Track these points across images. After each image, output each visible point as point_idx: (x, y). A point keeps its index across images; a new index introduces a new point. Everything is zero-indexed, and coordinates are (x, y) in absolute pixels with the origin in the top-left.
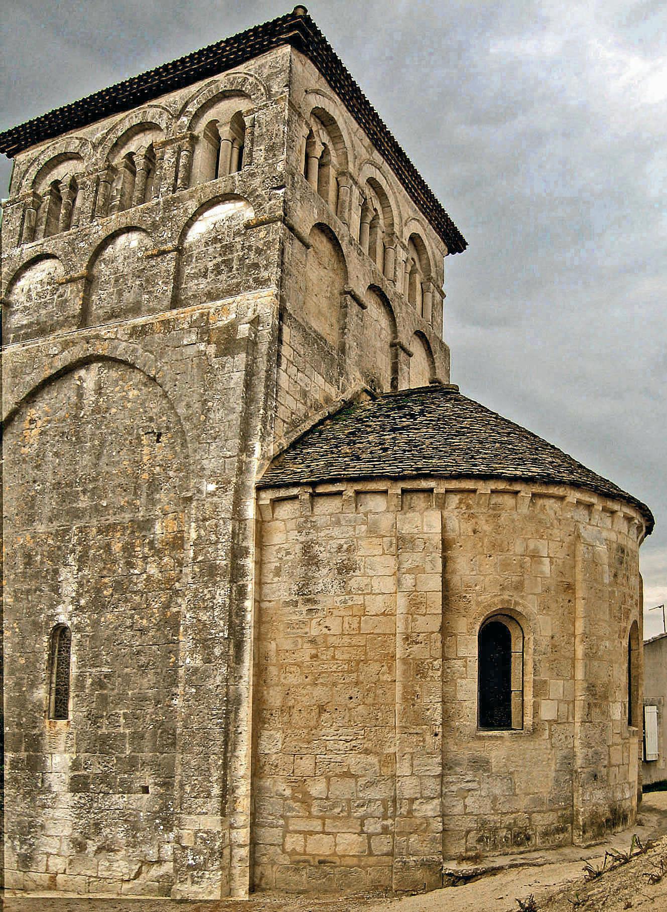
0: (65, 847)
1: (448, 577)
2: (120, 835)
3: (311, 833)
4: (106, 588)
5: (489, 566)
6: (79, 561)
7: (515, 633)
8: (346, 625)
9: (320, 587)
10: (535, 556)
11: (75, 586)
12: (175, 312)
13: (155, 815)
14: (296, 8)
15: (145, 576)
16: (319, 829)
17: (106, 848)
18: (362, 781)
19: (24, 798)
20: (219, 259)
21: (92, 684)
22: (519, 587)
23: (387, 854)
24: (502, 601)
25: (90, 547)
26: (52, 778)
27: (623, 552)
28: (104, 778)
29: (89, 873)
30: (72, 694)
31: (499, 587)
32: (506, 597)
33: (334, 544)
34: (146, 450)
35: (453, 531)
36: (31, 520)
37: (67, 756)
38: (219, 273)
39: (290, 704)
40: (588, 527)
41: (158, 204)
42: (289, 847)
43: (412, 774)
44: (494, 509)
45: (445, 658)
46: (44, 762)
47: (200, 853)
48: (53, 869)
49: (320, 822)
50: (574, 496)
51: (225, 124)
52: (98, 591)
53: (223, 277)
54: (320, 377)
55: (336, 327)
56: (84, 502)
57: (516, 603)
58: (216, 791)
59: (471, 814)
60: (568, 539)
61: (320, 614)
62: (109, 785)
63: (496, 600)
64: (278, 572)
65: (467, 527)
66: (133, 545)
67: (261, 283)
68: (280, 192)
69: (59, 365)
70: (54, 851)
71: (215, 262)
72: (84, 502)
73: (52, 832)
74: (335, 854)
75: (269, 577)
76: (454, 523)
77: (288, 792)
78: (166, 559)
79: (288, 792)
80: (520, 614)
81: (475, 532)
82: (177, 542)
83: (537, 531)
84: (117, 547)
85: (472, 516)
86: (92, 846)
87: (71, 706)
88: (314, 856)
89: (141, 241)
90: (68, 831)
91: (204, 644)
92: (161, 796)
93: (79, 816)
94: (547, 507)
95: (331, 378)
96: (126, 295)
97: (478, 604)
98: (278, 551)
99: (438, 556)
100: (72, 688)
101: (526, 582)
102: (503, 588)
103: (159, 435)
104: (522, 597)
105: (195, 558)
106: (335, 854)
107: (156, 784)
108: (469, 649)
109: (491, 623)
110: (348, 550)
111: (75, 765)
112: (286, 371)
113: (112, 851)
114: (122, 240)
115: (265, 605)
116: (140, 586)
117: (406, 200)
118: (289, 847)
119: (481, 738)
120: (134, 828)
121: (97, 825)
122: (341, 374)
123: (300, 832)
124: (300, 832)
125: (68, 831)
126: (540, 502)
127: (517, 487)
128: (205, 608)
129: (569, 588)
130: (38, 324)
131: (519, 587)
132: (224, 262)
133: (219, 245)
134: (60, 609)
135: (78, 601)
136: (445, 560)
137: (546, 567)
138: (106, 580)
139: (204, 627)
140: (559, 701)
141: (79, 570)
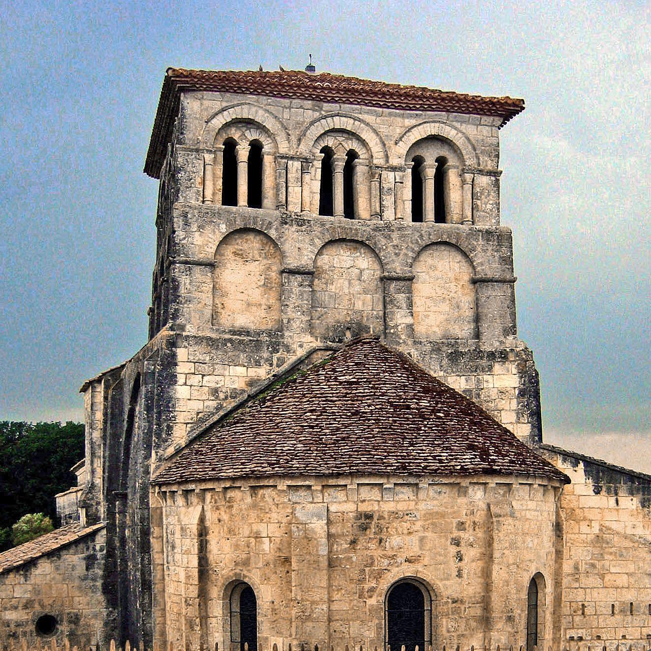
5: (227, 546)
10: (258, 537)
14: (167, 72)
22: (246, 563)
24: (236, 574)
31: (234, 563)
32: (237, 571)
44: (229, 502)
50: (282, 485)
57: (245, 576)
60: (285, 520)
63: (231, 574)
81: (219, 521)
83: (258, 517)
85: (218, 509)
94: (266, 496)
97: (222, 576)
101: (252, 558)
102: (237, 564)
104: (248, 571)
117: (379, 115)
127: (238, 484)
129: (287, 560)
131: (246, 563)
137: (266, 546)
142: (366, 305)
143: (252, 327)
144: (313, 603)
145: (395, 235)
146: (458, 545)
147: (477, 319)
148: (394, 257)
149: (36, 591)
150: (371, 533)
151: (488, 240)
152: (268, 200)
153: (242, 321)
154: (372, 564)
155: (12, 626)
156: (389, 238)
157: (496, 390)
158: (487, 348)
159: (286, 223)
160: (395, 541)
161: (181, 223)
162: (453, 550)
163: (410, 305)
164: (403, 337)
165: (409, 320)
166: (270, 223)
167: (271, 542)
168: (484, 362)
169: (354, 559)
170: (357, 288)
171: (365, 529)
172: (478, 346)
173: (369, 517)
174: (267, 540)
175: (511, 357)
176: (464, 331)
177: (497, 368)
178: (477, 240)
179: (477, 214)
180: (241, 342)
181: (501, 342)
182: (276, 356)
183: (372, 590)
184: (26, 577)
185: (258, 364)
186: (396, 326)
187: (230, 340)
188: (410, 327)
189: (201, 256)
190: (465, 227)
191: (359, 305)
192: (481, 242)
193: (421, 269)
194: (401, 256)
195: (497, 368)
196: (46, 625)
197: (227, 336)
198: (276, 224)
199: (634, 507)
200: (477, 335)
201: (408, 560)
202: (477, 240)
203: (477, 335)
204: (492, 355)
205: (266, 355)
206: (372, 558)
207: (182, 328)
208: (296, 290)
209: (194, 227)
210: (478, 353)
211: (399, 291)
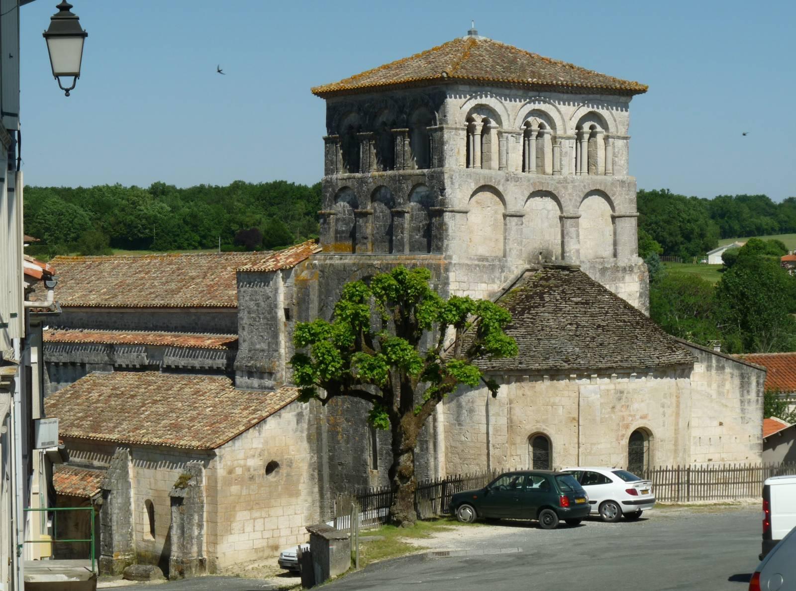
142: (552, 238)
143: (487, 254)
144: (592, 444)
145: (570, 186)
146: (663, 407)
147: (615, 244)
148: (569, 202)
149: (266, 442)
150: (623, 402)
151: (623, 187)
152: (495, 163)
153: (482, 251)
154: (624, 420)
155: (252, 470)
156: (565, 188)
157: (626, 294)
158: (621, 264)
159: (508, 180)
160: (635, 406)
161: (449, 183)
162: (661, 410)
163: (578, 236)
164: (574, 258)
165: (577, 247)
166: (499, 181)
167: (563, 408)
168: (620, 274)
169: (614, 417)
170: (546, 224)
171: (620, 399)
172: (616, 264)
173: (622, 392)
174: (561, 408)
175: (636, 270)
176: (608, 251)
177: (627, 277)
178: (616, 187)
179: (616, 168)
180: (484, 266)
181: (629, 260)
182: (503, 275)
183: (623, 436)
184: (259, 432)
185: (494, 282)
186: (570, 251)
187: (478, 266)
188: (578, 251)
189: (461, 206)
190: (609, 178)
191: (547, 237)
192: (619, 189)
193: (582, 211)
194: (573, 201)
195: (627, 277)
196: (271, 467)
197: (476, 262)
198: (503, 181)
199: (702, 371)
200: (615, 255)
201: (641, 418)
202: (616, 187)
203: (615, 255)
204: (624, 269)
205: (497, 275)
206: (623, 417)
207: (450, 257)
208: (514, 228)
209: (457, 186)
210: (616, 268)
211: (572, 226)
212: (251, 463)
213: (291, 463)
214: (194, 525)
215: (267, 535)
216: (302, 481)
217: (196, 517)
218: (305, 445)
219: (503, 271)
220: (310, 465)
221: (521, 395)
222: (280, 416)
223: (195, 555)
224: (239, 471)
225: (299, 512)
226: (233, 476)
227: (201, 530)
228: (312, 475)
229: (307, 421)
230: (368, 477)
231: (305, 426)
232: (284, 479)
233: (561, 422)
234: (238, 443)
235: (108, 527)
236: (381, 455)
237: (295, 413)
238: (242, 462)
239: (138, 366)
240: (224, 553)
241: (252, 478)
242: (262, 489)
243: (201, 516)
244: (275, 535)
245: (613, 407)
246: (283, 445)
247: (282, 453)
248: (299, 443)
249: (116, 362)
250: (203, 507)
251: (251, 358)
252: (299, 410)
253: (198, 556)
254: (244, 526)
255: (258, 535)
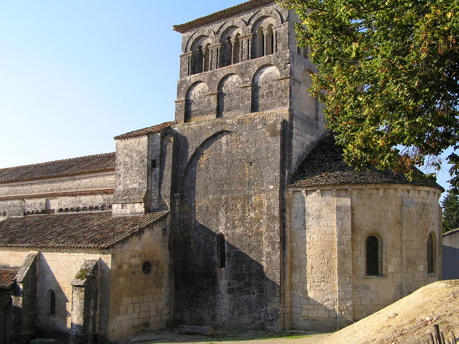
0: (227, 313)
1: (354, 221)
2: (246, 308)
3: (310, 310)
4: (236, 221)
6: (225, 210)
7: (379, 240)
8: (319, 238)
9: (310, 224)
11: (225, 219)
12: (253, 114)
13: (258, 302)
15: (249, 217)
16: (312, 308)
17: (241, 314)
18: (326, 293)
19: (212, 295)
20: (268, 91)
21: (233, 255)
23: (335, 318)
25: (229, 205)
26: (221, 289)
27: (424, 205)
28: (239, 289)
29: (236, 322)
30: (226, 259)
33: (314, 208)
34: (247, 169)
35: (355, 203)
36: (207, 193)
37: (226, 281)
38: (268, 97)
39: (302, 265)
40: (408, 198)
41: (242, 65)
42: (303, 315)
43: (342, 291)
45: (353, 250)
46: (218, 283)
47: (273, 316)
48: (223, 320)
49: (312, 306)
51: (266, 30)
52: (234, 222)
53: (270, 98)
54: (309, 135)
55: (314, 109)
56: (225, 188)
58: (278, 295)
59: (363, 305)
61: (310, 233)
62: (241, 292)
64: (296, 218)
65: (360, 202)
66: (245, 205)
67: (284, 105)
68: (289, 65)
69: (211, 133)
70: (223, 314)
71: (266, 92)
72: (225, 188)
73: (222, 307)
74: (318, 317)
75: (293, 219)
76: (355, 201)
77: (302, 296)
78: (257, 211)
79: (302, 296)
80: (380, 233)
82: (261, 205)
84: (239, 206)
85: (361, 198)
86: (236, 313)
87: (226, 263)
88: (311, 318)
89: (237, 79)
90: (228, 307)
91: (272, 244)
92: (259, 296)
93: (231, 302)
95: (313, 133)
96: (234, 102)
98: (296, 210)
99: (349, 214)
100: (226, 257)
103: (251, 163)
105: (267, 213)
106: (318, 317)
107: (257, 292)
108: (362, 248)
109: (373, 236)
110: (319, 211)
111: (229, 284)
112: (295, 139)
113: (244, 314)
114: (230, 79)
115: (292, 229)
116: (248, 221)
118: (303, 315)
119: (366, 278)
120: (250, 307)
121: (238, 305)
122: (317, 130)
123: (306, 309)
124: (306, 309)
125: (228, 307)
126: (388, 191)
128: (272, 231)
130: (200, 110)
132: (269, 92)
133: (267, 84)
134: (220, 227)
135: (226, 225)
136: (352, 216)
138: (236, 217)
139: (271, 238)
140: (396, 265)
141: (226, 213)
155: (133, 267)
212: (133, 261)
213: (158, 263)
214: (90, 307)
215: (142, 315)
216: (164, 277)
217: (92, 302)
218: (167, 251)
219: (317, 130)
220: (170, 266)
221: (361, 204)
222: (153, 229)
223: (90, 331)
224: (125, 267)
225: (162, 299)
226: (121, 270)
227: (95, 312)
228: (171, 273)
229: (168, 235)
230: (217, 273)
231: (167, 238)
232: (154, 274)
233: (390, 224)
234: (126, 246)
235: (303, 267)
236: (229, 256)
237: (161, 228)
238: (127, 260)
239: (40, 211)
240: (113, 330)
241: (133, 273)
242: (140, 281)
243: (96, 301)
244: (147, 316)
245: (421, 215)
246: (154, 250)
247: (153, 256)
248: (164, 250)
249: (26, 210)
250: (97, 293)
251: (125, 194)
252: (164, 226)
253: (93, 332)
254: (127, 308)
255: (136, 315)
